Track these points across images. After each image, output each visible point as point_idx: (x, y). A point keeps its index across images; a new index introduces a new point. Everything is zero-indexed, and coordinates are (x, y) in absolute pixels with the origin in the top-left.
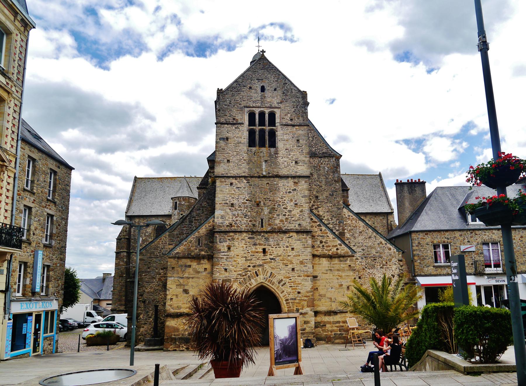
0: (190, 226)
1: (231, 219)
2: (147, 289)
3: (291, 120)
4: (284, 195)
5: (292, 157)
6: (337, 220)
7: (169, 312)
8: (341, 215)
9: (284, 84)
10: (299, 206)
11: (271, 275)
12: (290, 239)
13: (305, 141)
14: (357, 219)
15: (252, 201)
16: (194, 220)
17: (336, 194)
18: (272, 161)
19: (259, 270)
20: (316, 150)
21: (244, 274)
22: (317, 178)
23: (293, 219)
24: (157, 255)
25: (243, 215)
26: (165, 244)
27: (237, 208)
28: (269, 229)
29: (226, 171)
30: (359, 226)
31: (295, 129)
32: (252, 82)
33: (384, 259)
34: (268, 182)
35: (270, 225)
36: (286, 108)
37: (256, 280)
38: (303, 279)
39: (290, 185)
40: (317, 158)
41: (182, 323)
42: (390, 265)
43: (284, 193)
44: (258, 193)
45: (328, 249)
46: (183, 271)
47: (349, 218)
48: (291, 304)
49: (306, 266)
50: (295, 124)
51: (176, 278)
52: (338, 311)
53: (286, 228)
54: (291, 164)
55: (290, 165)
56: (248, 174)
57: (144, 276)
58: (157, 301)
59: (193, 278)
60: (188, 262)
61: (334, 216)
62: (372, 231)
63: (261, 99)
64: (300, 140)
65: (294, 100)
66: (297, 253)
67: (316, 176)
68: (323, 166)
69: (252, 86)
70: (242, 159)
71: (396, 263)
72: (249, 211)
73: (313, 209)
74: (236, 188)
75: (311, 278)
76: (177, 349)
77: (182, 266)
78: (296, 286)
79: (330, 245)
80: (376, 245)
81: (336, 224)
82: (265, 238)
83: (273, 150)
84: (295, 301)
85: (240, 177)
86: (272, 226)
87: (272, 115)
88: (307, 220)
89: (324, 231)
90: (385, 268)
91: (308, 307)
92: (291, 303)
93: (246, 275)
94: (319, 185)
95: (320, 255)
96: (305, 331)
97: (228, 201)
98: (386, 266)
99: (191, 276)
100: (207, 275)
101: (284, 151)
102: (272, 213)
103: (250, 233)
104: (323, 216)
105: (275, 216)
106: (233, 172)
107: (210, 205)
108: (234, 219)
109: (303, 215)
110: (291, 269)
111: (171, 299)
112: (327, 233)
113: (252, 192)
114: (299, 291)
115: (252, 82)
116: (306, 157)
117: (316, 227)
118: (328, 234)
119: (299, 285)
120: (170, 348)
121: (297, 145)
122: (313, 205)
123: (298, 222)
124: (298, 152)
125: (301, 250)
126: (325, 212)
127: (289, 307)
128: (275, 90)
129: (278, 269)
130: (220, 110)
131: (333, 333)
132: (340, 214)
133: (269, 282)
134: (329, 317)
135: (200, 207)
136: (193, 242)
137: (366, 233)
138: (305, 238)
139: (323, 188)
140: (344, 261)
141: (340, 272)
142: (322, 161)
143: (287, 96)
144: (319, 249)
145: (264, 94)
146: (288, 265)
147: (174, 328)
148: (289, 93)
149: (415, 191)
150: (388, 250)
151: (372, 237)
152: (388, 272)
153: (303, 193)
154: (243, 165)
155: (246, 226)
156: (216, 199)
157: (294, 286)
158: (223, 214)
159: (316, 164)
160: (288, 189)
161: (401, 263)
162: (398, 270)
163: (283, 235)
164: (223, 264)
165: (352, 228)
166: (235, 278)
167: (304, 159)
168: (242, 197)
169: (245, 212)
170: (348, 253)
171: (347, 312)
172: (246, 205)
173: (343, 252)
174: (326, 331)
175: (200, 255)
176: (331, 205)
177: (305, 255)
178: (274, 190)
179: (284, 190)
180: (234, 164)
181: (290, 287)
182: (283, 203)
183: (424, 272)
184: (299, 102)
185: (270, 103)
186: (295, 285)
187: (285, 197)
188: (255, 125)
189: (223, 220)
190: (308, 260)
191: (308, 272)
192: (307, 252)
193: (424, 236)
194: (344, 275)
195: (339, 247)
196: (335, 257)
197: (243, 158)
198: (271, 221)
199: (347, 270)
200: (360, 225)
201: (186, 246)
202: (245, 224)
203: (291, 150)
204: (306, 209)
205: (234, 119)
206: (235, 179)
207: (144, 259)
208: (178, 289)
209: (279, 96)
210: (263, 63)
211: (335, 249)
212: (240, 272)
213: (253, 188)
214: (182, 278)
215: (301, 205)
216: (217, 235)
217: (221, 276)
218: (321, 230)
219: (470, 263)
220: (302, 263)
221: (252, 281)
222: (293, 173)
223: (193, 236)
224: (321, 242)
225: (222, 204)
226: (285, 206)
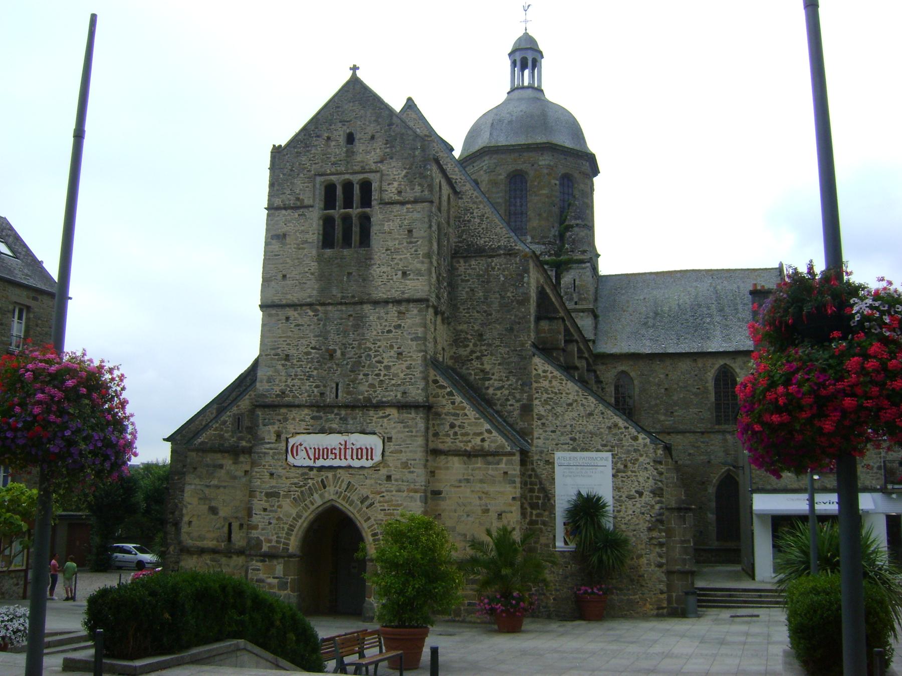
1: (284, 384)
3: (400, 193)
6: (519, 379)
11: (347, 488)
12: (385, 420)
14: (563, 377)
15: (322, 350)
19: (327, 477)
20: (485, 242)
21: (301, 483)
22: (482, 298)
23: (393, 382)
25: (305, 375)
30: (568, 391)
31: (405, 210)
33: (620, 458)
35: (349, 393)
36: (390, 170)
37: (322, 496)
38: (406, 497)
40: (484, 259)
42: (632, 472)
43: (378, 333)
45: (465, 439)
47: (544, 377)
49: (413, 472)
51: (199, 487)
53: (378, 399)
55: (392, 279)
56: (318, 300)
57: (177, 480)
59: (225, 487)
60: (219, 458)
61: (512, 372)
62: (595, 402)
63: (347, 156)
64: (414, 230)
66: (396, 447)
67: (481, 294)
68: (495, 273)
69: (330, 135)
70: (307, 272)
71: (648, 466)
72: (315, 369)
73: (472, 359)
74: (295, 326)
75: (421, 496)
78: (393, 510)
79: (469, 431)
80: (605, 431)
81: (515, 389)
82: (341, 419)
83: (362, 251)
85: (301, 305)
87: (366, 187)
88: (419, 383)
89: (459, 404)
90: (622, 477)
93: (305, 485)
94: (485, 312)
95: (449, 451)
97: (279, 350)
98: (624, 472)
101: (383, 253)
102: (355, 371)
103: (315, 409)
104: (491, 372)
105: (361, 377)
108: (288, 383)
109: (411, 374)
110: (385, 477)
111: (190, 523)
112: (464, 408)
116: (423, 262)
117: (443, 397)
118: (466, 411)
119: (398, 508)
122: (472, 352)
123: (402, 388)
124: (408, 254)
126: (495, 364)
128: (373, 138)
129: (362, 477)
133: (344, 499)
136: (228, 423)
137: (583, 405)
138: (413, 419)
139: (493, 316)
141: (485, 485)
142: (493, 264)
146: (379, 470)
150: (630, 440)
152: (629, 486)
153: (413, 331)
155: (309, 396)
159: (482, 270)
160: (386, 326)
161: (661, 468)
162: (651, 482)
165: (552, 396)
166: (286, 490)
167: (419, 266)
169: (308, 370)
173: (493, 445)
175: (238, 446)
176: (508, 349)
177: (411, 451)
179: (379, 327)
180: (294, 282)
181: (381, 510)
183: (770, 484)
186: (391, 508)
187: (379, 340)
188: (352, 208)
189: (270, 384)
190: (417, 461)
191: (416, 484)
195: (486, 435)
196: (476, 456)
197: (310, 270)
203: (397, 251)
205: (298, 199)
211: (478, 439)
212: (296, 480)
214: (208, 486)
215: (409, 355)
217: (264, 486)
218: (453, 403)
219: (876, 466)
220: (405, 465)
221: (316, 496)
222: (396, 295)
224: (452, 426)
225: (270, 355)
226: (379, 357)
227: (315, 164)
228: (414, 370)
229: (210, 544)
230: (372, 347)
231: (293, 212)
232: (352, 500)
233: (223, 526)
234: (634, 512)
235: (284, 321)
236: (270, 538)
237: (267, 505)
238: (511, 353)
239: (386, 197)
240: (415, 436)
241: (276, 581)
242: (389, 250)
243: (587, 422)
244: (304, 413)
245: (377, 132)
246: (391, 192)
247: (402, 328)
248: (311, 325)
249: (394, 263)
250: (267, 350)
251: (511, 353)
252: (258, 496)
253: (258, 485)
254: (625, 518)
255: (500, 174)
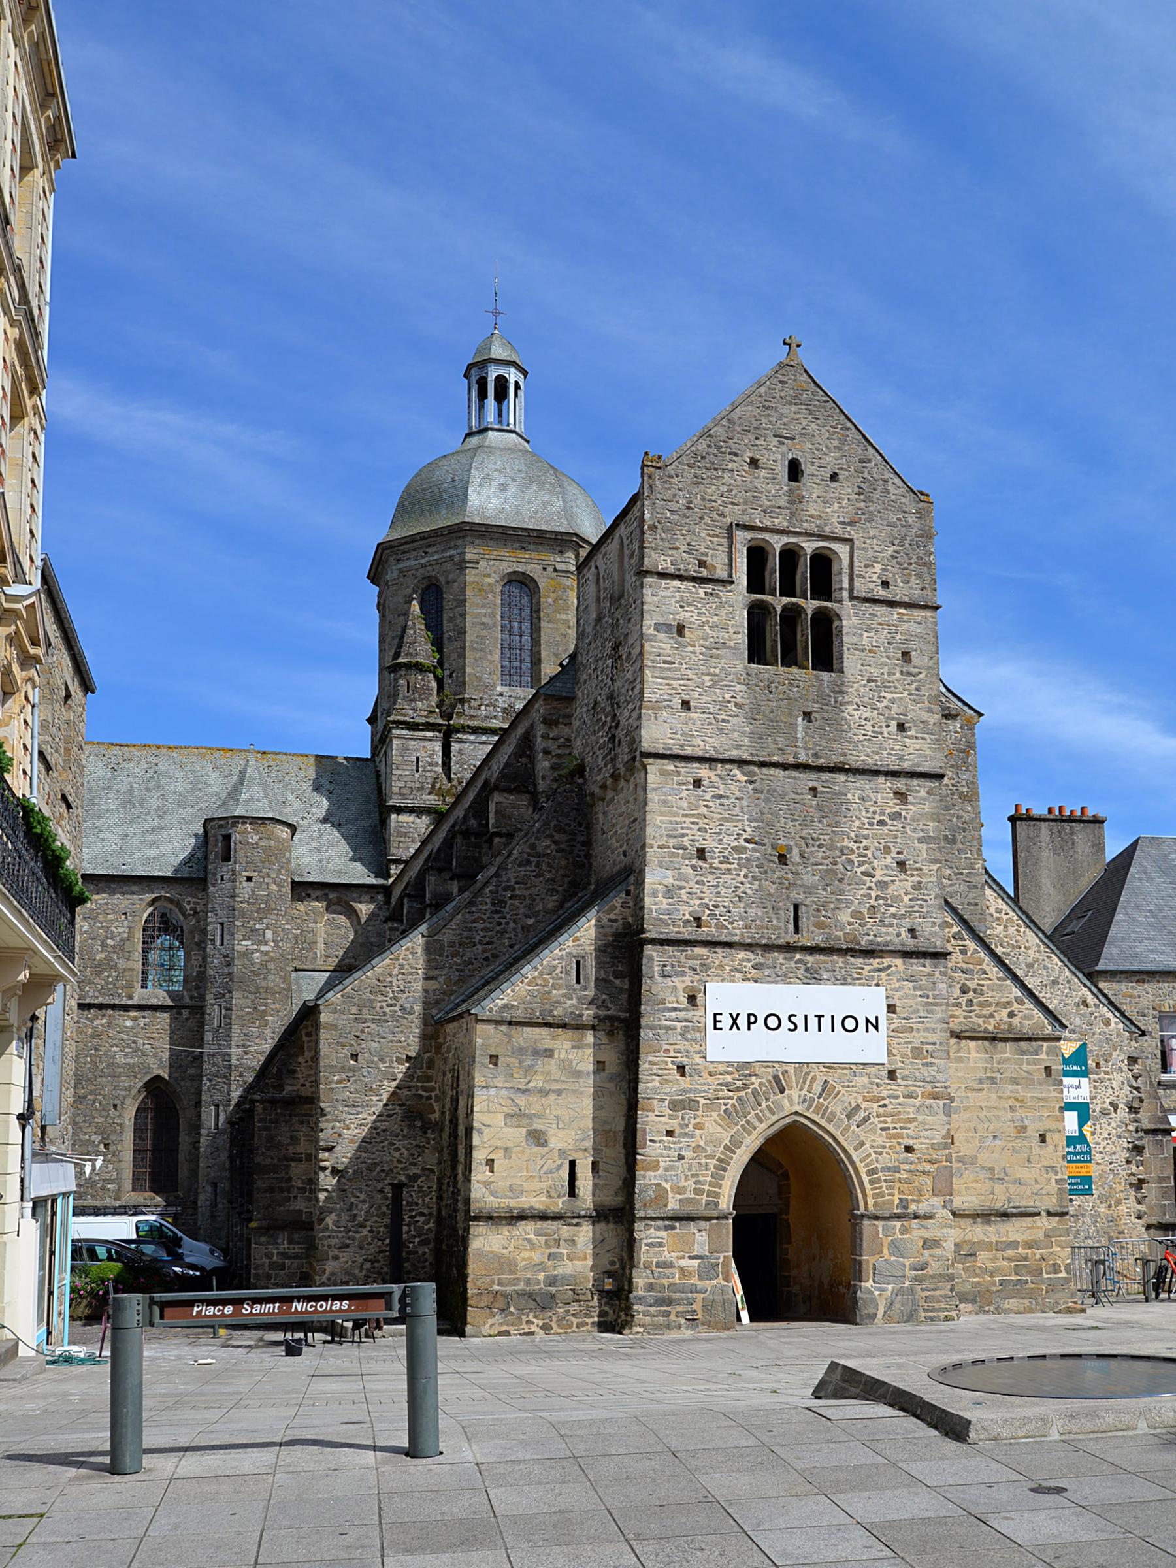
0: (496, 916)
2: (348, 1129)
4: (865, 832)
5: (887, 707)
7: (483, 1205)
8: (979, 907)
9: (861, 461)
10: (911, 869)
11: (823, 1090)
12: (883, 975)
13: (926, 658)
16: (510, 898)
17: (964, 837)
18: (826, 715)
19: (787, 1072)
21: (739, 1083)
23: (893, 910)
24: (385, 1014)
26: (411, 974)
27: (716, 863)
28: (818, 939)
29: (679, 736)
30: (1027, 945)
32: (758, 442)
34: (815, 784)
35: (820, 925)
39: (882, 798)
41: (526, 1243)
42: (1107, 1073)
43: (864, 824)
44: (783, 820)
45: (986, 1011)
46: (529, 1070)
47: (998, 919)
48: (883, 1184)
49: (932, 1064)
50: (897, 598)
51: (504, 1093)
52: (1015, 1211)
53: (871, 938)
54: (885, 730)
57: (340, 1082)
58: (383, 1171)
59: (559, 1093)
65: (893, 518)
66: (903, 1021)
70: (729, 702)
74: (713, 797)
75: (945, 1104)
76: (511, 1329)
77: (521, 1051)
78: (901, 1128)
82: (807, 970)
84: (897, 1175)
86: (827, 930)
87: (823, 564)
91: (934, 1195)
92: (886, 1181)
96: (925, 1272)
97: (686, 839)
99: (555, 1087)
100: (608, 1085)
101: (865, 686)
106: (702, 743)
107: (563, 850)
109: (922, 899)
111: (490, 1162)
113: (762, 813)
114: (910, 1142)
115: (758, 442)
116: (930, 711)
118: (984, 966)
119: (909, 1125)
120: (487, 1326)
121: (904, 670)
125: (918, 1011)
127: (877, 1194)
130: (656, 527)
131: (997, 1279)
132: (976, 904)
134: (986, 1227)
135: (529, 854)
136: (558, 971)
137: (1045, 968)
138: (929, 975)
140: (1031, 1053)
143: (872, 501)
144: (956, 1013)
145: (798, 488)
147: (498, 1257)
148: (876, 495)
149: (1073, 844)
151: (1061, 981)
153: (921, 827)
154: (734, 720)
156: (649, 831)
157: (895, 1128)
158: (671, 880)
160: (874, 813)
163: (861, 960)
164: (671, 1048)
166: (710, 1096)
167: (925, 716)
168: (732, 829)
170: (1043, 1027)
171: (1038, 1214)
172: (744, 856)
174: (978, 1271)
177: (927, 1030)
178: (833, 810)
179: (864, 813)
180: (705, 716)
181: (882, 1129)
182: (860, 855)
184: (908, 526)
185: (818, 522)
191: (937, 1085)
192: (935, 1019)
193: (1132, 988)
194: (1032, 1097)
197: (733, 697)
198: (823, 913)
199: (1040, 1083)
200: (1027, 941)
201: (537, 985)
202: (741, 919)
203: (885, 686)
204: (931, 879)
205: (702, 564)
206: (710, 769)
207: (336, 1027)
208: (511, 1130)
209: (846, 501)
210: (795, 380)
212: (728, 1078)
213: (767, 801)
214: (524, 1092)
215: (917, 865)
216: (649, 950)
217: (667, 1088)
220: (917, 1052)
222: (893, 764)
223: (557, 951)
227: (732, 503)
228: (926, 892)
229: (538, 1202)
230: (854, 848)
231: (694, 587)
232: (831, 1112)
233: (560, 1166)
234: (1109, 1135)
235: (691, 787)
236: (682, 1184)
237: (674, 1125)
238: (953, 877)
239: (861, 588)
240: (934, 1004)
241: (696, 1262)
242: (873, 681)
243: (1052, 993)
244: (739, 956)
245: (842, 469)
246: (868, 583)
247: (903, 820)
248: (743, 798)
249: (883, 704)
250: (661, 836)
251: (953, 877)
252: (656, 1109)
253: (655, 1087)
254: (1099, 1144)
255: (489, 575)
